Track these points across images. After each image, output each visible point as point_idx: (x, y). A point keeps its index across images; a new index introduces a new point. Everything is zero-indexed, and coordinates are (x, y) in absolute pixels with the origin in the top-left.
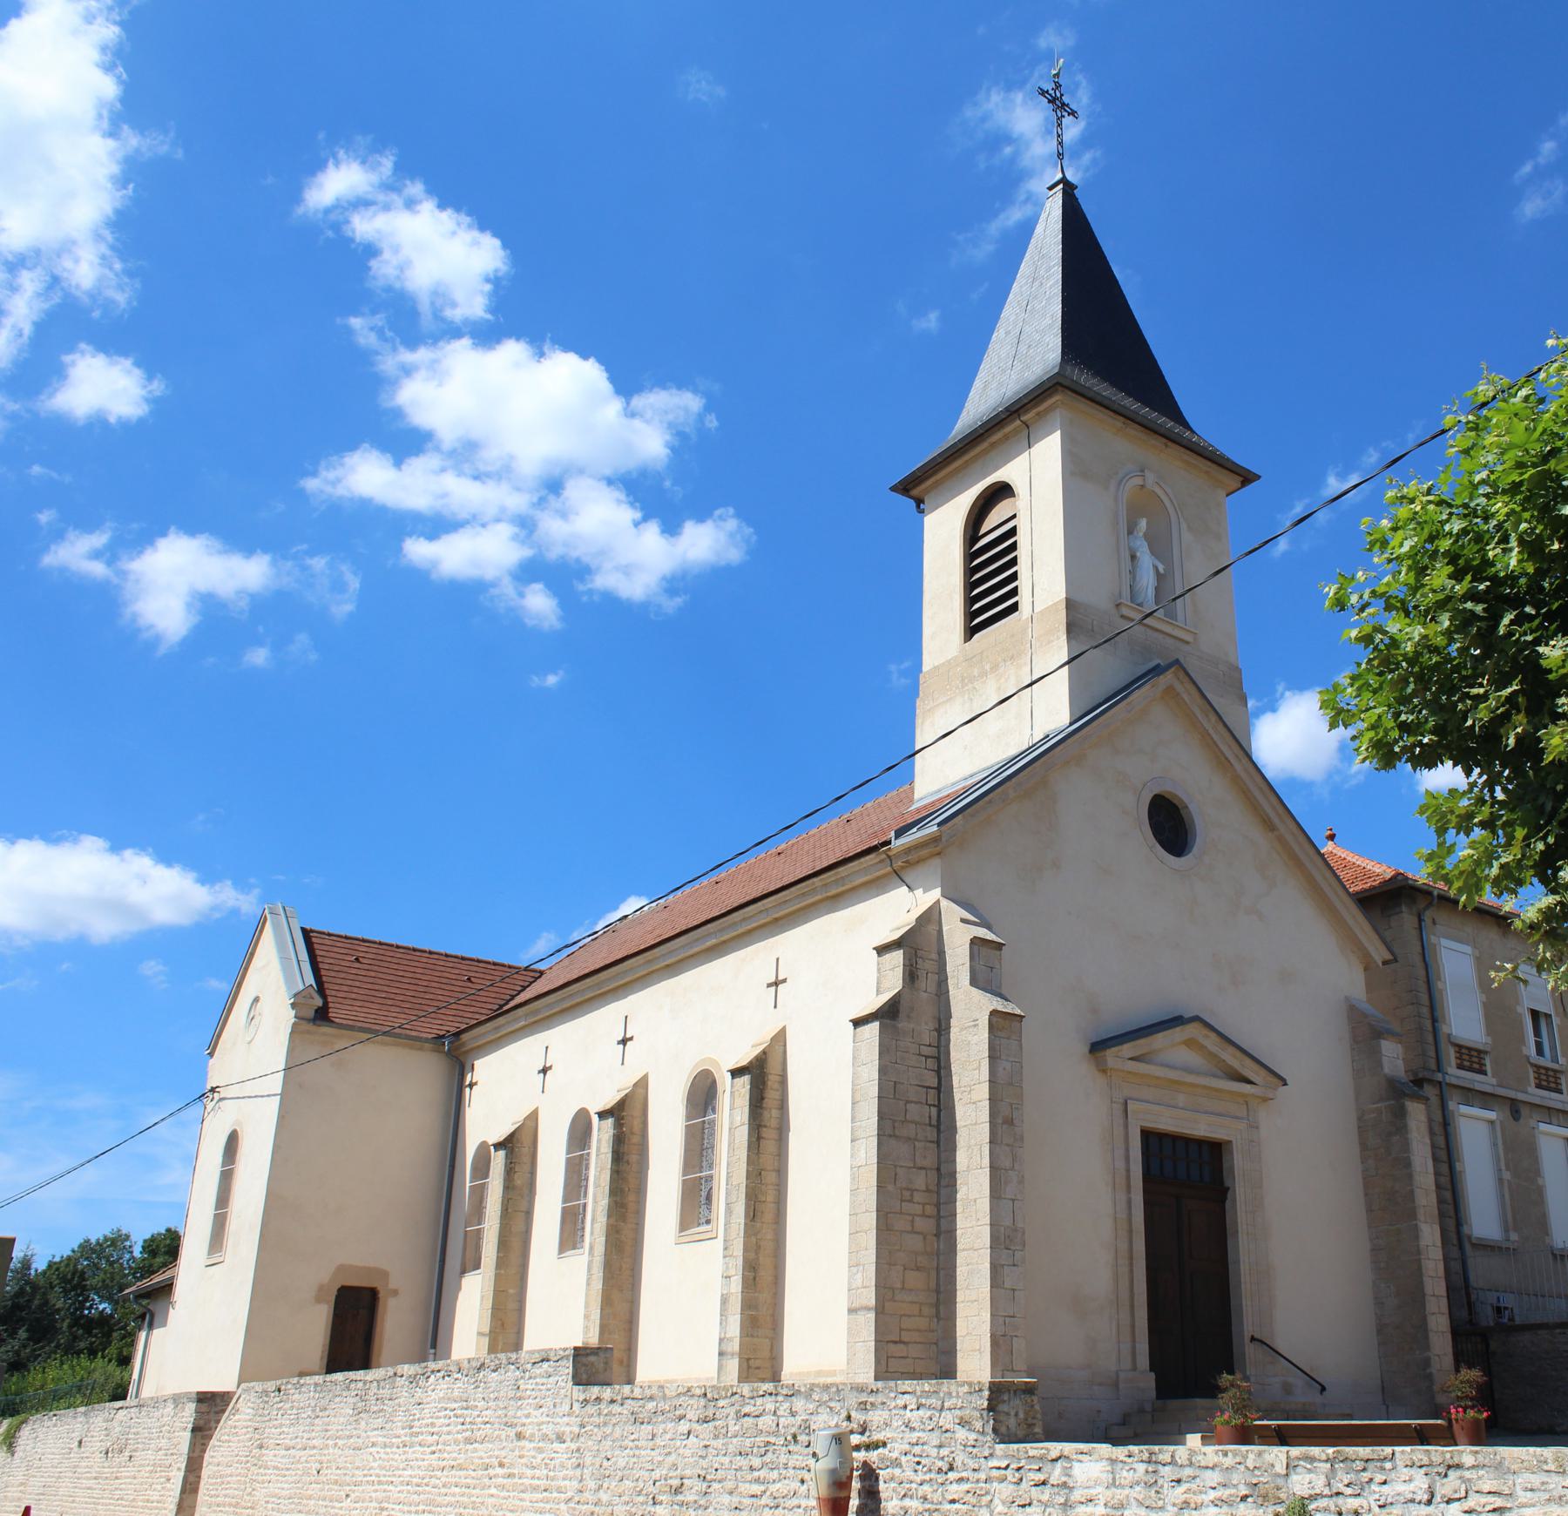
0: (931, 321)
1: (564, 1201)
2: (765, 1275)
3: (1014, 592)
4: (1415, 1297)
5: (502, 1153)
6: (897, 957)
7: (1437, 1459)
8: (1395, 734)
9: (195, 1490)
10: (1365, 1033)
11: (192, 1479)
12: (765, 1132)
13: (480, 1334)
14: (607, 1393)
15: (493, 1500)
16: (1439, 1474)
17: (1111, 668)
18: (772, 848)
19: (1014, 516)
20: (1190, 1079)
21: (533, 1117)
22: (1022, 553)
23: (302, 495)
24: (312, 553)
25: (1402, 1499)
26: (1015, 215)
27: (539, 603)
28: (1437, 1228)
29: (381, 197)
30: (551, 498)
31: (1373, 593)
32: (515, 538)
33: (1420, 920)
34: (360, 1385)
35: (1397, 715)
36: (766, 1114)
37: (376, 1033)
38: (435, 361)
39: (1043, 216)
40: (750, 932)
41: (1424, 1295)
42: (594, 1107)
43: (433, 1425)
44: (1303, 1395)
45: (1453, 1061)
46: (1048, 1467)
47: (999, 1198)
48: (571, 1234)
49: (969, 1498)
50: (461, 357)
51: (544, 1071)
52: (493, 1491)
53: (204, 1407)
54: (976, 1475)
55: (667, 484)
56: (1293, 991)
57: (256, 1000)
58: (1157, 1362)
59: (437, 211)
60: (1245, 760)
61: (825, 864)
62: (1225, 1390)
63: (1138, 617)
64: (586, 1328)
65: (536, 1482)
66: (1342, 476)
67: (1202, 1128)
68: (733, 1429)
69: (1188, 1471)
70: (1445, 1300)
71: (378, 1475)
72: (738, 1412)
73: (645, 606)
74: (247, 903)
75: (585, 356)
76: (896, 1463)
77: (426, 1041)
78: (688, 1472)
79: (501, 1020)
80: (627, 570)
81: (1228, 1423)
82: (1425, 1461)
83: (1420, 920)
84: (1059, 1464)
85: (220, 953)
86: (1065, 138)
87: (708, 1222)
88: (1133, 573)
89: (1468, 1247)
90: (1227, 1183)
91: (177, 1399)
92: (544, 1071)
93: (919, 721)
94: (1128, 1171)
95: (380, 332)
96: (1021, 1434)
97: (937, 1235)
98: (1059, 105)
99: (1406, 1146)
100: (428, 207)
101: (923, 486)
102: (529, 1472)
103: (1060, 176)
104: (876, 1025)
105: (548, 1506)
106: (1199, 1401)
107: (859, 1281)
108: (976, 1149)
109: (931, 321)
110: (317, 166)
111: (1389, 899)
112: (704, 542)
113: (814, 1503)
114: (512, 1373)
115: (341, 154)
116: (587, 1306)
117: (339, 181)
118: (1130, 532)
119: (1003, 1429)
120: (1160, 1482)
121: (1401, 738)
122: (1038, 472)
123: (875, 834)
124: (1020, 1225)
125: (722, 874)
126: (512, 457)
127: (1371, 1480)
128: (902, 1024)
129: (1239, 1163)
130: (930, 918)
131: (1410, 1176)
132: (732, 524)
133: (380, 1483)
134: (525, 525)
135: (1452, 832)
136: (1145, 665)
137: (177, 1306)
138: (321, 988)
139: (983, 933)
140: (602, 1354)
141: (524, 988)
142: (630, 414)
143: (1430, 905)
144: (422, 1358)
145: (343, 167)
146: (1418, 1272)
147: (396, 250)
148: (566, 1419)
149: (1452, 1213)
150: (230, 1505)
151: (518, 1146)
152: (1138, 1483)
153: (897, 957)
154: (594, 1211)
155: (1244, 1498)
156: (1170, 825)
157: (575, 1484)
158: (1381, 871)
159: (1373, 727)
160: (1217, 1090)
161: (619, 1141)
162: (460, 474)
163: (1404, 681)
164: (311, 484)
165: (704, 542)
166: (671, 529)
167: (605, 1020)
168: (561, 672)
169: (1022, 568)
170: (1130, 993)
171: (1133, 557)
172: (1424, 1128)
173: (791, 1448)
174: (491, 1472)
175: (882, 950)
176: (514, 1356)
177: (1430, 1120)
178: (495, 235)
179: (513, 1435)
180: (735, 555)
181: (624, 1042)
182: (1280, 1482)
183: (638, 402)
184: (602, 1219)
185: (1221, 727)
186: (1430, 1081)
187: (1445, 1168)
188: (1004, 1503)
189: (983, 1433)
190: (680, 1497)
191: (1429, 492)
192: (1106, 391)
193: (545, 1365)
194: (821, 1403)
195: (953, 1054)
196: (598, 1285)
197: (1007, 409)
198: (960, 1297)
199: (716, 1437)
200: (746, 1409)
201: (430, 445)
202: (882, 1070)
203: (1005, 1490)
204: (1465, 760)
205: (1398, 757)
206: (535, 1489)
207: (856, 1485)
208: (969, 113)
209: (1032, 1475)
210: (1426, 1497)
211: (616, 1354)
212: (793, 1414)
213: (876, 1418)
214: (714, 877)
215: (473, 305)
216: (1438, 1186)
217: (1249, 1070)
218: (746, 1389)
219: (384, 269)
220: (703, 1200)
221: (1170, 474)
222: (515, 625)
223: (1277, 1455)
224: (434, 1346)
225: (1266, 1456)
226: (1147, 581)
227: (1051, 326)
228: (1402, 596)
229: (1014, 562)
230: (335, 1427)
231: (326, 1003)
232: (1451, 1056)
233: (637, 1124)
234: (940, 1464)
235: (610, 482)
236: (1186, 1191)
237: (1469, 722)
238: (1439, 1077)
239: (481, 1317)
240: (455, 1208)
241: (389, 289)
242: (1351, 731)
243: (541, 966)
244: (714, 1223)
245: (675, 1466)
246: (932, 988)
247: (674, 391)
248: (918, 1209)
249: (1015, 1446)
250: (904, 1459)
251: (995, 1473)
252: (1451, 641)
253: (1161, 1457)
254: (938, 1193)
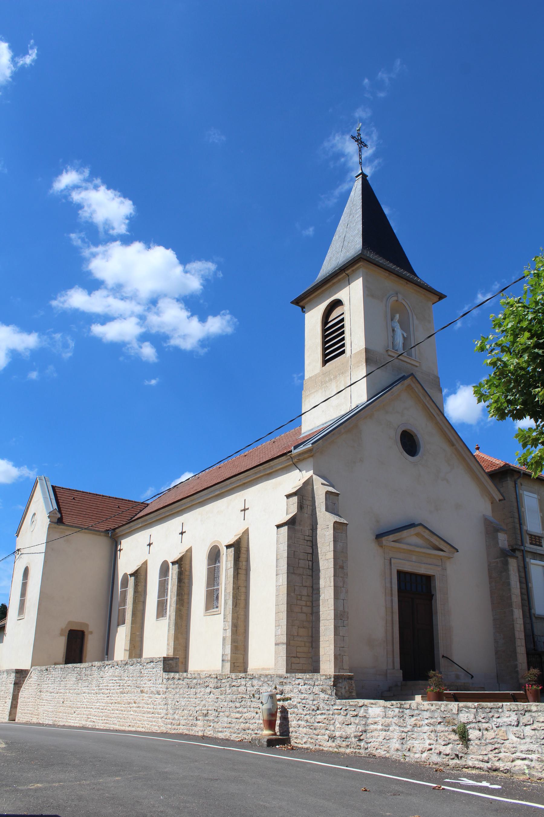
0: (311, 231)
1: (159, 598)
2: (241, 630)
3: (343, 345)
4: (511, 639)
5: (133, 578)
6: (295, 499)
7: (521, 708)
8: (505, 405)
9: (16, 707)
10: (491, 530)
11: (14, 703)
12: (240, 571)
13: (125, 650)
14: (177, 676)
15: (132, 716)
16: (521, 714)
17: (384, 377)
18: (242, 454)
19: (343, 314)
20: (418, 549)
21: (145, 563)
22: (347, 329)
23: (51, 308)
24: (55, 332)
25: (506, 724)
26: (346, 187)
27: (148, 351)
28: (521, 611)
29: (84, 185)
30: (152, 307)
31: (496, 344)
32: (138, 324)
33: (515, 484)
34: (78, 669)
35: (507, 396)
36: (240, 563)
37: (82, 528)
38: (106, 251)
39: (354, 188)
40: (233, 489)
41: (515, 638)
42: (170, 561)
43: (107, 686)
44: (464, 680)
45: (528, 541)
46: (358, 709)
47: (338, 599)
48: (161, 611)
49: (325, 721)
50: (117, 250)
51: (150, 545)
52: (132, 713)
53: (18, 675)
54: (328, 712)
55: (202, 301)
56: (461, 514)
57: (34, 514)
58: (403, 667)
59: (106, 190)
60: (441, 416)
61: (265, 460)
62: (431, 678)
63: (396, 356)
64: (168, 649)
65: (149, 710)
66: (484, 294)
67: (422, 570)
68: (228, 691)
69: (416, 712)
70: (524, 640)
71: (86, 705)
72: (230, 685)
73: (192, 352)
74: (32, 474)
75: (167, 248)
76: (295, 707)
77: (102, 532)
78: (210, 708)
79: (132, 524)
80: (184, 337)
81: (432, 691)
82: (516, 709)
83: (515, 484)
84: (363, 708)
85: (22, 493)
86: (363, 157)
87: (217, 607)
88: (393, 337)
89: (534, 619)
90: (433, 592)
91: (8, 672)
92: (150, 545)
93: (303, 400)
94: (391, 587)
95: (83, 240)
96: (347, 696)
97: (312, 614)
98: (361, 144)
99: (508, 577)
100: (103, 188)
101: (305, 301)
102: (146, 706)
103: (360, 171)
104: (286, 527)
105: (154, 720)
106: (420, 682)
107: (279, 632)
108: (328, 579)
109: (311, 231)
110: (58, 173)
111: (503, 475)
112: (216, 325)
113: (261, 722)
114: (139, 667)
115: (69, 168)
116: (168, 640)
117: (68, 179)
118: (392, 320)
119: (339, 694)
120: (405, 716)
121: (508, 406)
122: (353, 296)
123: (285, 448)
124: (346, 610)
125: (222, 464)
126: (137, 290)
127: (493, 716)
128: (297, 527)
129: (438, 584)
130: (309, 483)
131: (510, 590)
132: (228, 317)
133: (87, 708)
134: (142, 318)
135: (529, 446)
136: (400, 376)
137: (7, 635)
138: (60, 511)
139: (331, 489)
140: (174, 660)
141: (141, 511)
142: (186, 272)
143: (519, 477)
144: (102, 660)
145: (69, 174)
146: (513, 629)
147: (90, 206)
148: (160, 685)
149: (527, 604)
150: (29, 713)
151: (139, 575)
152: (395, 716)
153: (295, 499)
154: (170, 602)
155: (440, 723)
156: (409, 443)
157: (164, 711)
158: (499, 462)
159: (496, 402)
160: (430, 554)
161: (180, 574)
162: (115, 297)
163: (509, 382)
164: (54, 303)
165: (216, 325)
166: (203, 319)
167: (173, 525)
168: (158, 379)
169: (347, 335)
170: (392, 513)
171: (393, 330)
172: (516, 569)
173: (252, 700)
174: (131, 705)
175: (288, 496)
176: (139, 660)
177: (518, 566)
178: (130, 199)
179: (139, 691)
180: (229, 330)
181: (182, 533)
182: (455, 716)
183: (189, 267)
184: (174, 606)
185: (431, 402)
186: (519, 550)
187: (524, 586)
188: (340, 723)
189: (331, 695)
190: (207, 718)
191: (519, 302)
192: (381, 260)
193: (152, 664)
194: (264, 682)
195: (318, 539)
196: (172, 632)
197: (339, 269)
198: (321, 639)
199: (221, 694)
200: (234, 684)
201: (103, 286)
202: (289, 546)
203: (340, 718)
204: (535, 416)
205: (507, 414)
206: (149, 713)
207: (279, 715)
208: (326, 144)
209: (351, 712)
210: (516, 723)
211: (181, 660)
212: (253, 686)
213: (287, 688)
214: (218, 466)
215: (121, 228)
216: (521, 593)
217: (442, 546)
218: (233, 676)
219: (84, 214)
220: (215, 598)
221: (409, 296)
222: (139, 361)
223: (454, 706)
224: (107, 654)
225: (449, 706)
226: (399, 340)
227: (357, 234)
228: (508, 346)
229: (343, 333)
230: (69, 685)
231: (62, 516)
232: (527, 539)
233: (187, 567)
234: (313, 707)
235: (178, 300)
236: (415, 596)
237: (537, 399)
238: (522, 548)
239: (125, 644)
240: (116, 599)
241: (87, 222)
242: (487, 403)
243: (148, 502)
244: (219, 608)
245: (205, 706)
246: (309, 512)
247: (204, 262)
248: (304, 603)
249: (345, 701)
250: (298, 705)
251: (336, 711)
252: (529, 365)
253: (405, 706)
254: (312, 597)
